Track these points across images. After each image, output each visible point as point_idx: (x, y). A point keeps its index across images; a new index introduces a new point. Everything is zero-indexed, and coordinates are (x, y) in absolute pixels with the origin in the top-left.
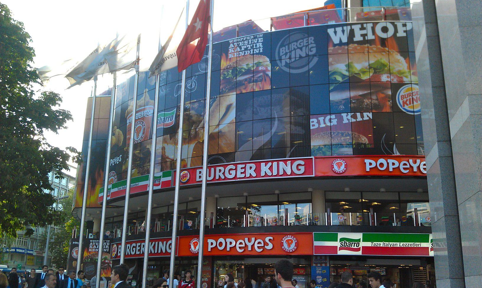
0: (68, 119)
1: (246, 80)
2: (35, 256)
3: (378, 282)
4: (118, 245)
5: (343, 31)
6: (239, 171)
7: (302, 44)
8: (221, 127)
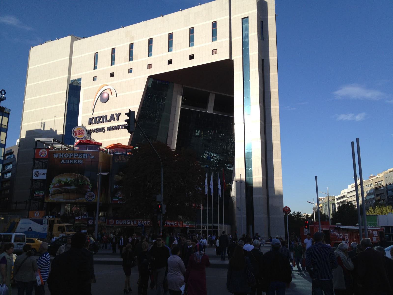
0: (83, 126)
5: (57, 155)
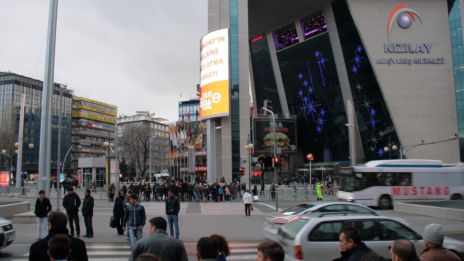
1: (204, 131)
2: (154, 166)
3: (79, 140)
4: (152, 157)
6: (203, 153)
7: (202, 153)
8: (199, 142)
